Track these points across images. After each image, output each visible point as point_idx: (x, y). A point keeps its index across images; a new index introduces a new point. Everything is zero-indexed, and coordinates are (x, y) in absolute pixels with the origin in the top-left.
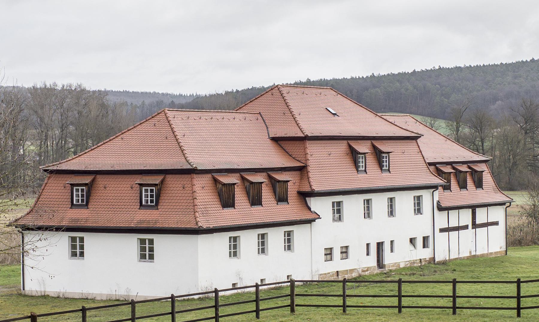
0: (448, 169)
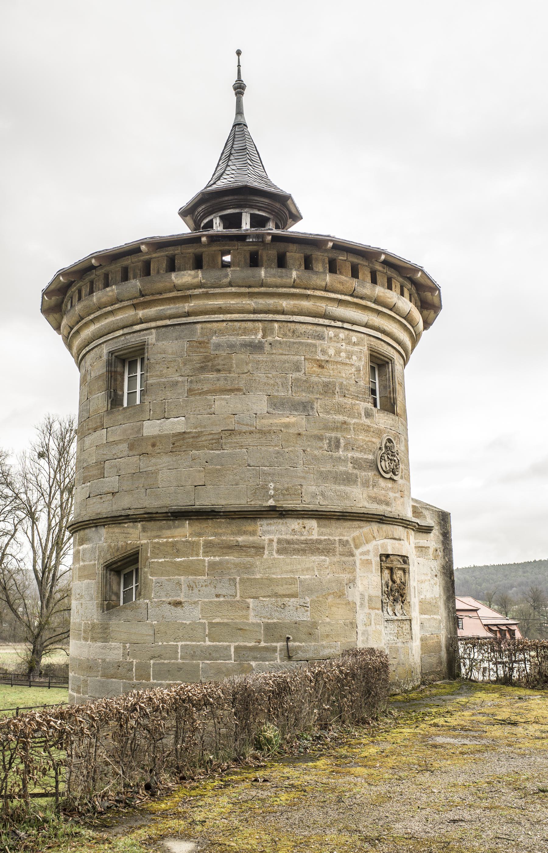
0: (495, 628)
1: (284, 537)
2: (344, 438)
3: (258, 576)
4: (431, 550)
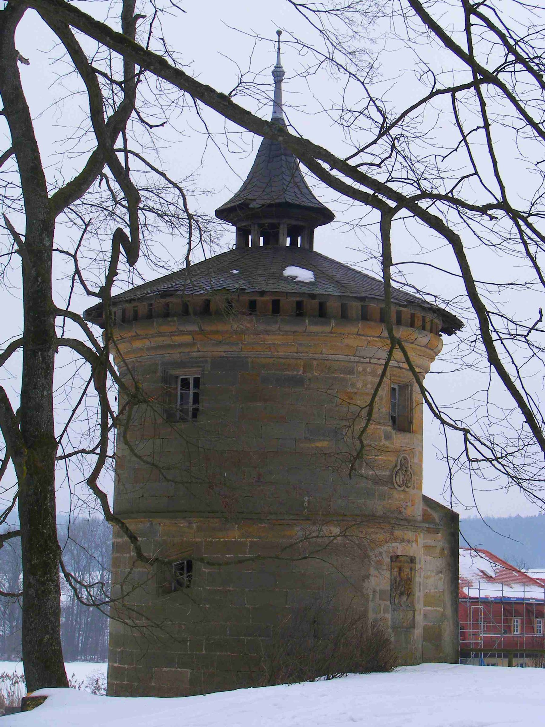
4: (438, 550)
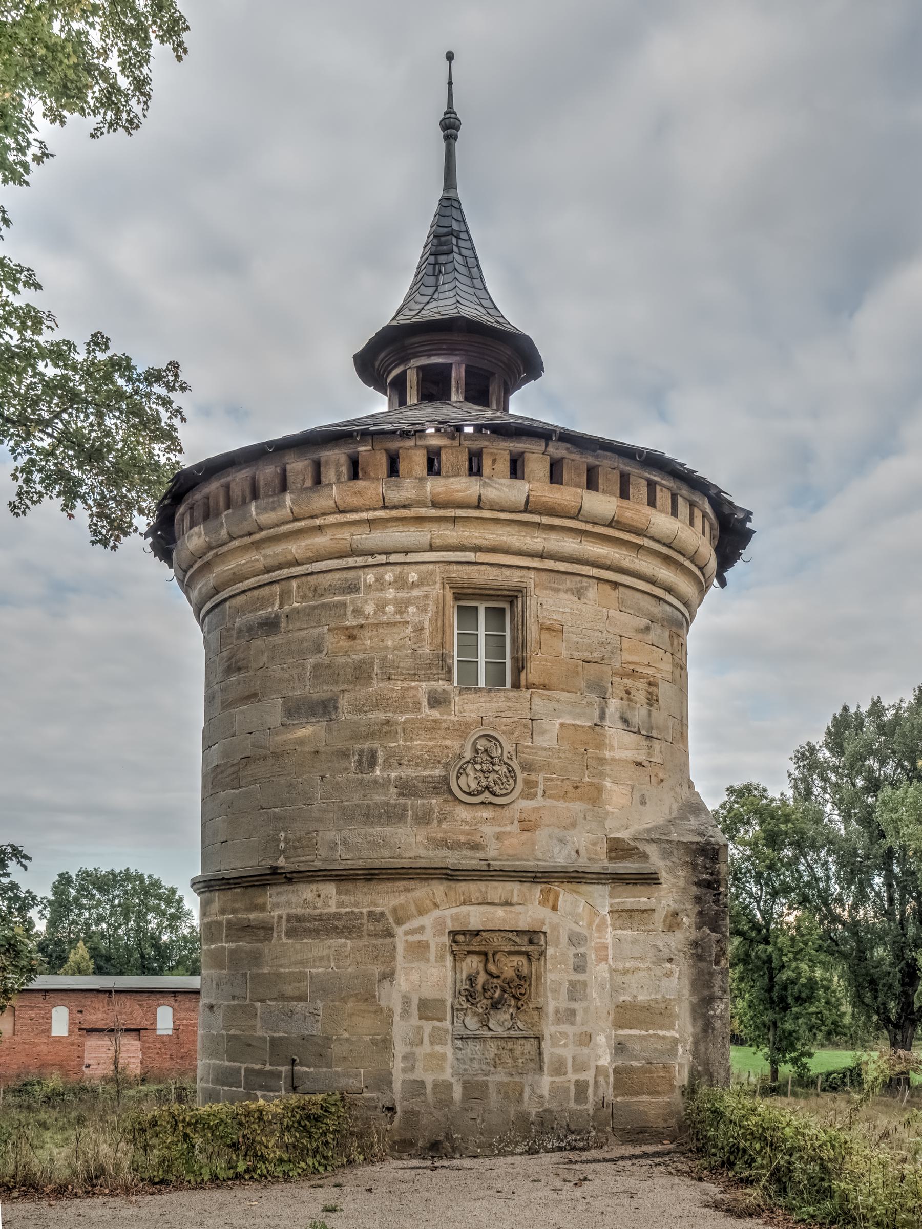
1: (294, 911)
2: (385, 747)
3: (266, 971)
